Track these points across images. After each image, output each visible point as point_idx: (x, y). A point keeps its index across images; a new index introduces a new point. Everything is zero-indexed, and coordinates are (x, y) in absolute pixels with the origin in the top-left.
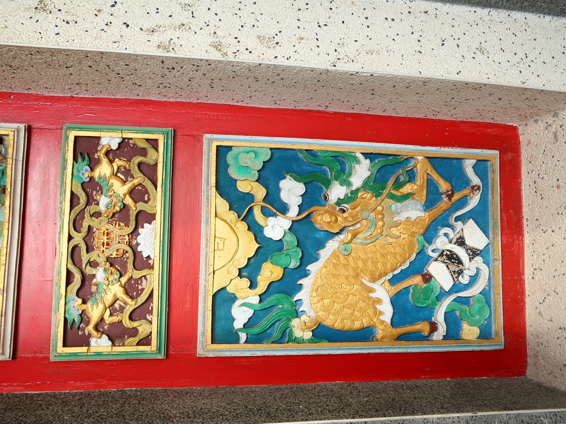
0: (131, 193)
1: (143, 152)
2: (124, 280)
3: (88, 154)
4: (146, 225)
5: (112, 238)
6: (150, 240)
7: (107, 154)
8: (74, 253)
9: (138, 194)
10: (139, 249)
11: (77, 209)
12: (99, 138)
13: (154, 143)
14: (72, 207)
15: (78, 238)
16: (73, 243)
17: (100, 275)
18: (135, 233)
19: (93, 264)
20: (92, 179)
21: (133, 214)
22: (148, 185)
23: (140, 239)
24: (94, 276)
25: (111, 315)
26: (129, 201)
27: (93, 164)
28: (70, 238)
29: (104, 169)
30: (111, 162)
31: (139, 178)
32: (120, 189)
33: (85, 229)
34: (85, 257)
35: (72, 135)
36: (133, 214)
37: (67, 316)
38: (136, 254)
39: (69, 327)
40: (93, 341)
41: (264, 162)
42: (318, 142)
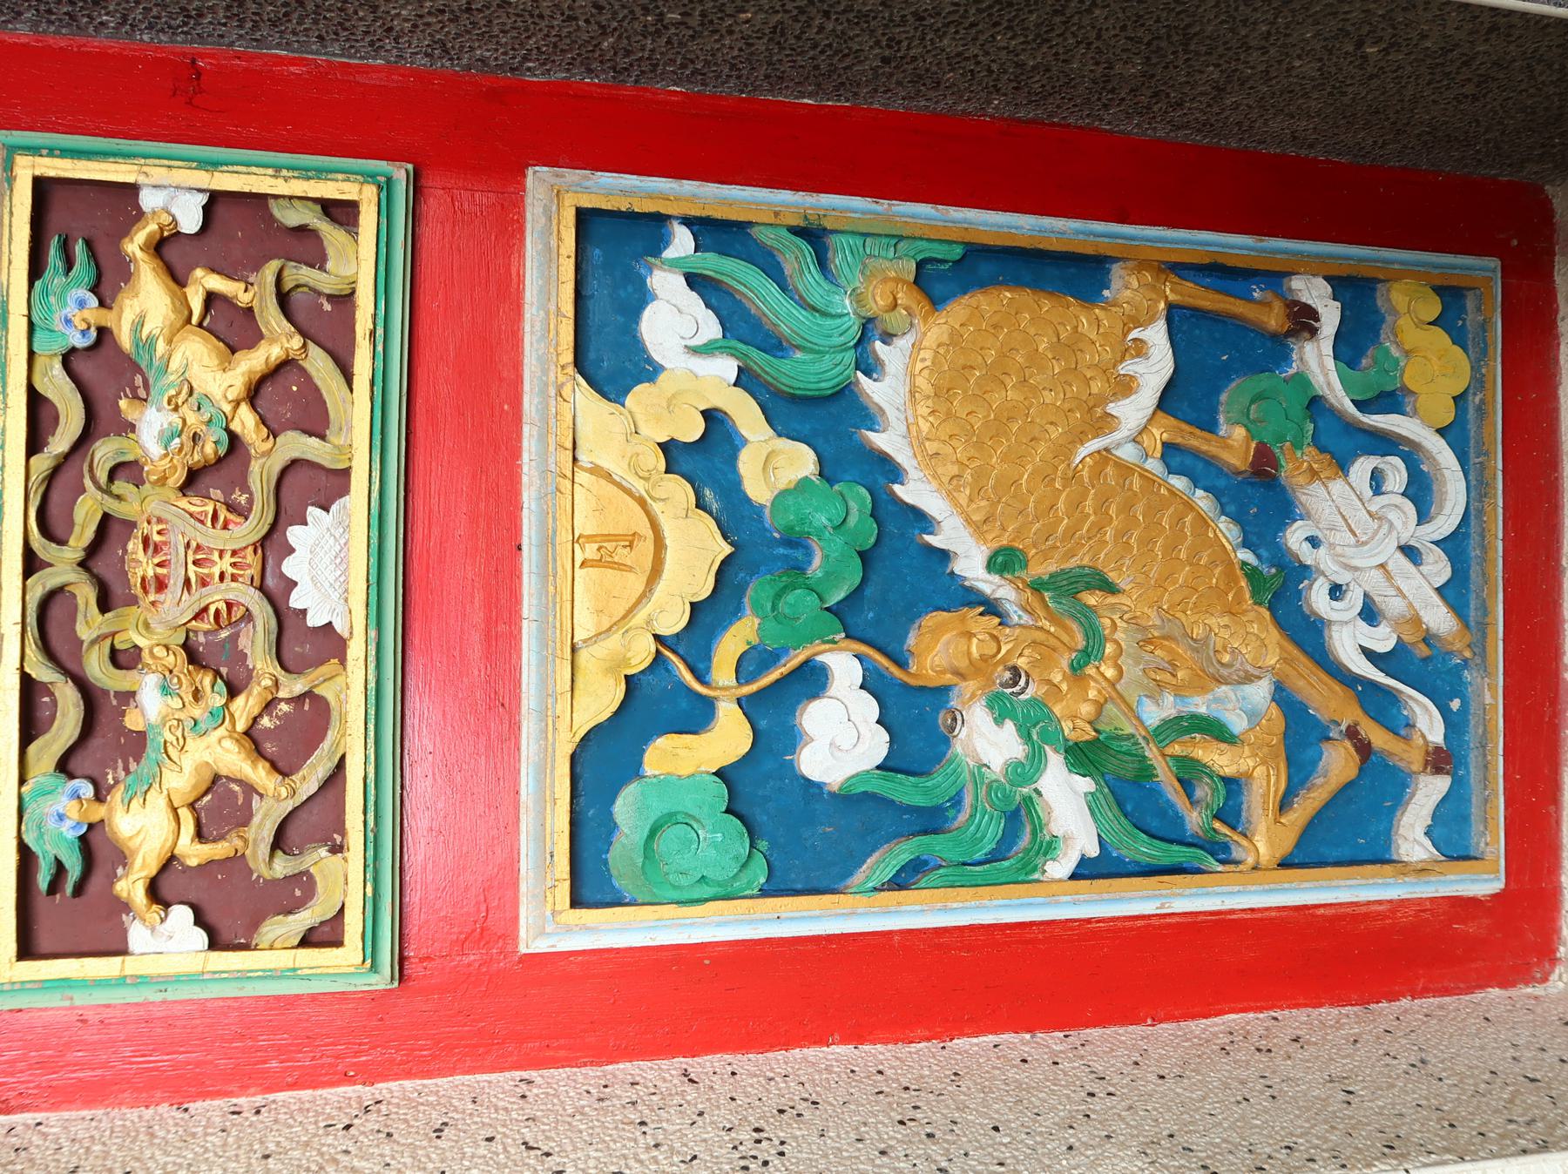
0: (253, 394)
1: (306, 247)
2: (244, 707)
3: (89, 244)
4: (313, 512)
5: (189, 554)
6: (330, 570)
7: (159, 247)
8: (47, 621)
9: (282, 396)
10: (296, 601)
11: (60, 443)
12: (132, 189)
13: (342, 213)
14: (34, 445)
15: (63, 566)
16: (41, 584)
17: (151, 703)
18: (272, 543)
19: (122, 659)
20: (104, 334)
21: (261, 474)
22: (319, 364)
23: (290, 567)
24: (128, 696)
25: (200, 835)
26: (246, 422)
27: (107, 284)
28: (31, 564)
29: (147, 305)
30: (177, 278)
31: (279, 341)
32: (216, 377)
33: (83, 534)
34: (89, 624)
35: (26, 170)
36: (261, 474)
37: (29, 839)
38: (285, 619)
39: (43, 880)
40: (137, 935)
41: (1454, 398)
42: (1264, 244)
